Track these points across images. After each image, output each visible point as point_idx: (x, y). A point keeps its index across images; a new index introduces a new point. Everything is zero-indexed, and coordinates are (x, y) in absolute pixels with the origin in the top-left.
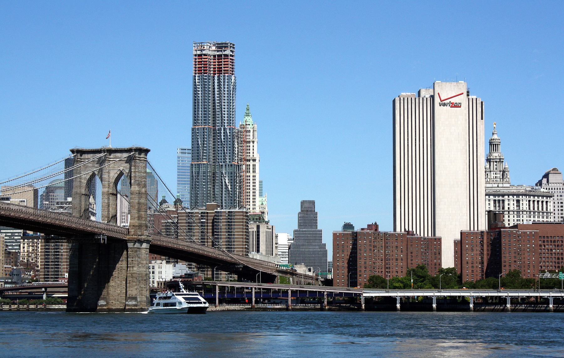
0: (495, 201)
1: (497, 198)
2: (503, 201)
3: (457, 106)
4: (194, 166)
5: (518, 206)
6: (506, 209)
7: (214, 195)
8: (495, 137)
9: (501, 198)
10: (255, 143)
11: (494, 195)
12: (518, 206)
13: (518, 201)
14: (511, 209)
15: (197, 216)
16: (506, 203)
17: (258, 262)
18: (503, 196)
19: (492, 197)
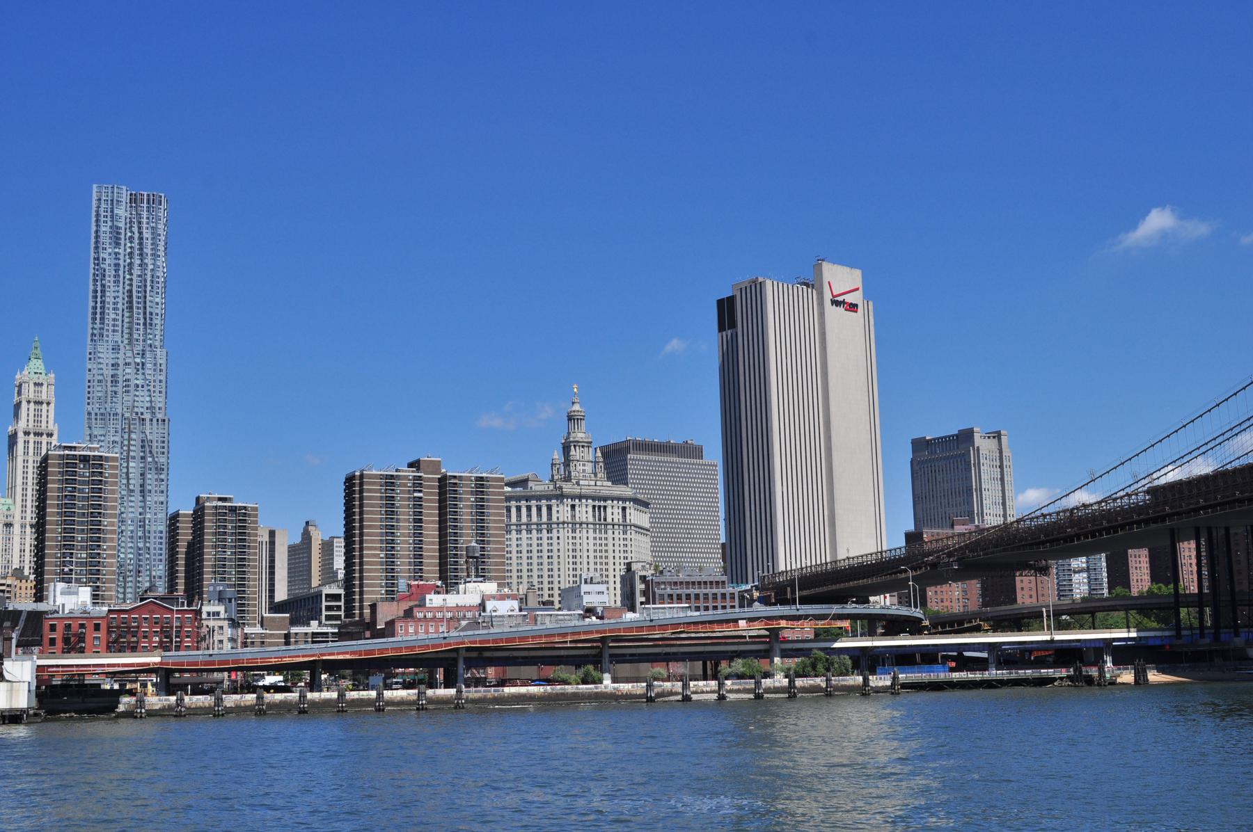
0: (594, 507)
1: (597, 503)
2: (605, 507)
3: (853, 307)
4: (93, 416)
5: (624, 516)
6: (609, 520)
7: (127, 474)
8: (577, 407)
9: (602, 503)
10: (52, 405)
11: (594, 499)
12: (624, 516)
13: (624, 509)
14: (616, 521)
15: (405, 485)
16: (609, 510)
17: (728, 564)
18: (605, 499)
19: (590, 501)
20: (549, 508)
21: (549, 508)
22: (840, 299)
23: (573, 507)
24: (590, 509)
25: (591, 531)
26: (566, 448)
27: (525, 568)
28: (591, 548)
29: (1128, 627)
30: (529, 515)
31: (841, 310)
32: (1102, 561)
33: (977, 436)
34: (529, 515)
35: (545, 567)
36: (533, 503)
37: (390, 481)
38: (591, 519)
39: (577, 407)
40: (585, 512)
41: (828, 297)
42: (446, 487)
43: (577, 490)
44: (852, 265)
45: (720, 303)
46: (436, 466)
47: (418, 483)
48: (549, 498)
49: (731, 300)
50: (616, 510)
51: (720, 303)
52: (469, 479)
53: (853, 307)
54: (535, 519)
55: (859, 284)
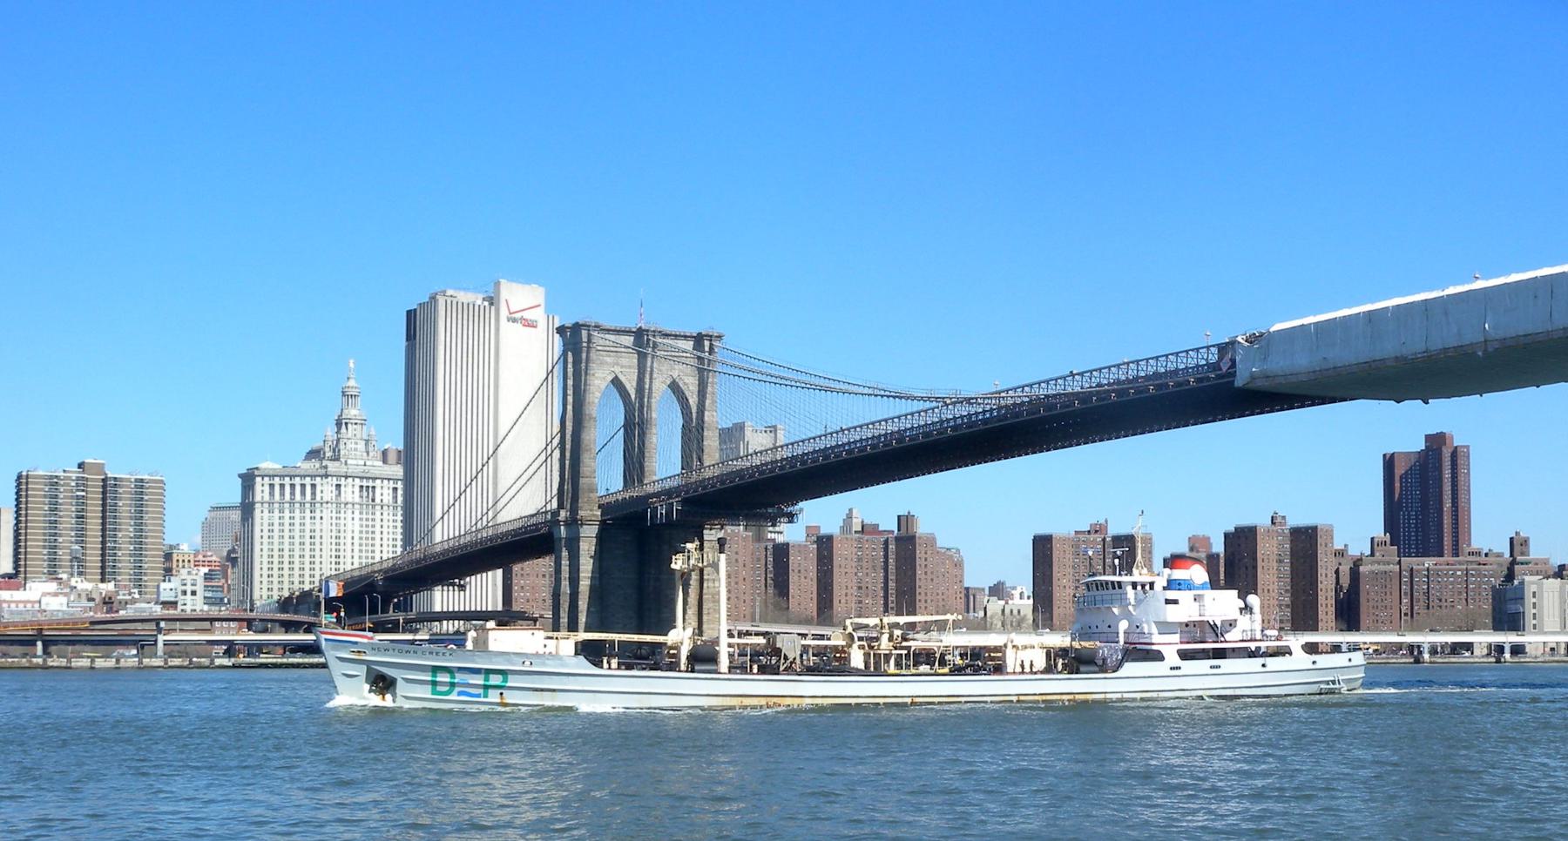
3: (531, 324)
6: (378, 500)
8: (352, 383)
9: (371, 484)
16: (378, 491)
18: (374, 479)
20: (313, 486)
21: (313, 486)
22: (518, 316)
23: (338, 486)
24: (357, 489)
26: (339, 424)
27: (286, 547)
28: (357, 529)
29: (753, 620)
30: (293, 493)
31: (519, 326)
32: (500, 572)
33: (748, 433)
34: (293, 493)
35: (307, 547)
36: (308, 481)
37: (53, 482)
38: (357, 499)
39: (352, 383)
40: (351, 492)
41: (504, 313)
42: (108, 488)
43: (343, 470)
44: (528, 280)
45: (409, 312)
46: (99, 468)
47: (82, 483)
48: (313, 477)
50: (385, 491)
51: (409, 312)
52: (129, 480)
53: (531, 324)
54: (298, 497)
55: (541, 300)
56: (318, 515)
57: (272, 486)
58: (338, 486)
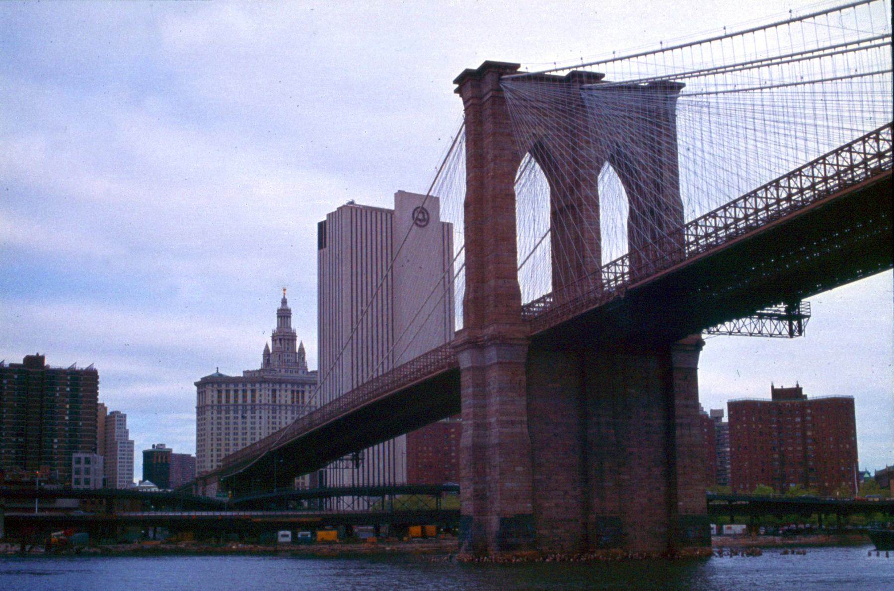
16: (307, 394)
23: (274, 391)
25: (289, 413)
49: (325, 222)
56: (257, 414)
57: (219, 392)
58: (274, 391)
